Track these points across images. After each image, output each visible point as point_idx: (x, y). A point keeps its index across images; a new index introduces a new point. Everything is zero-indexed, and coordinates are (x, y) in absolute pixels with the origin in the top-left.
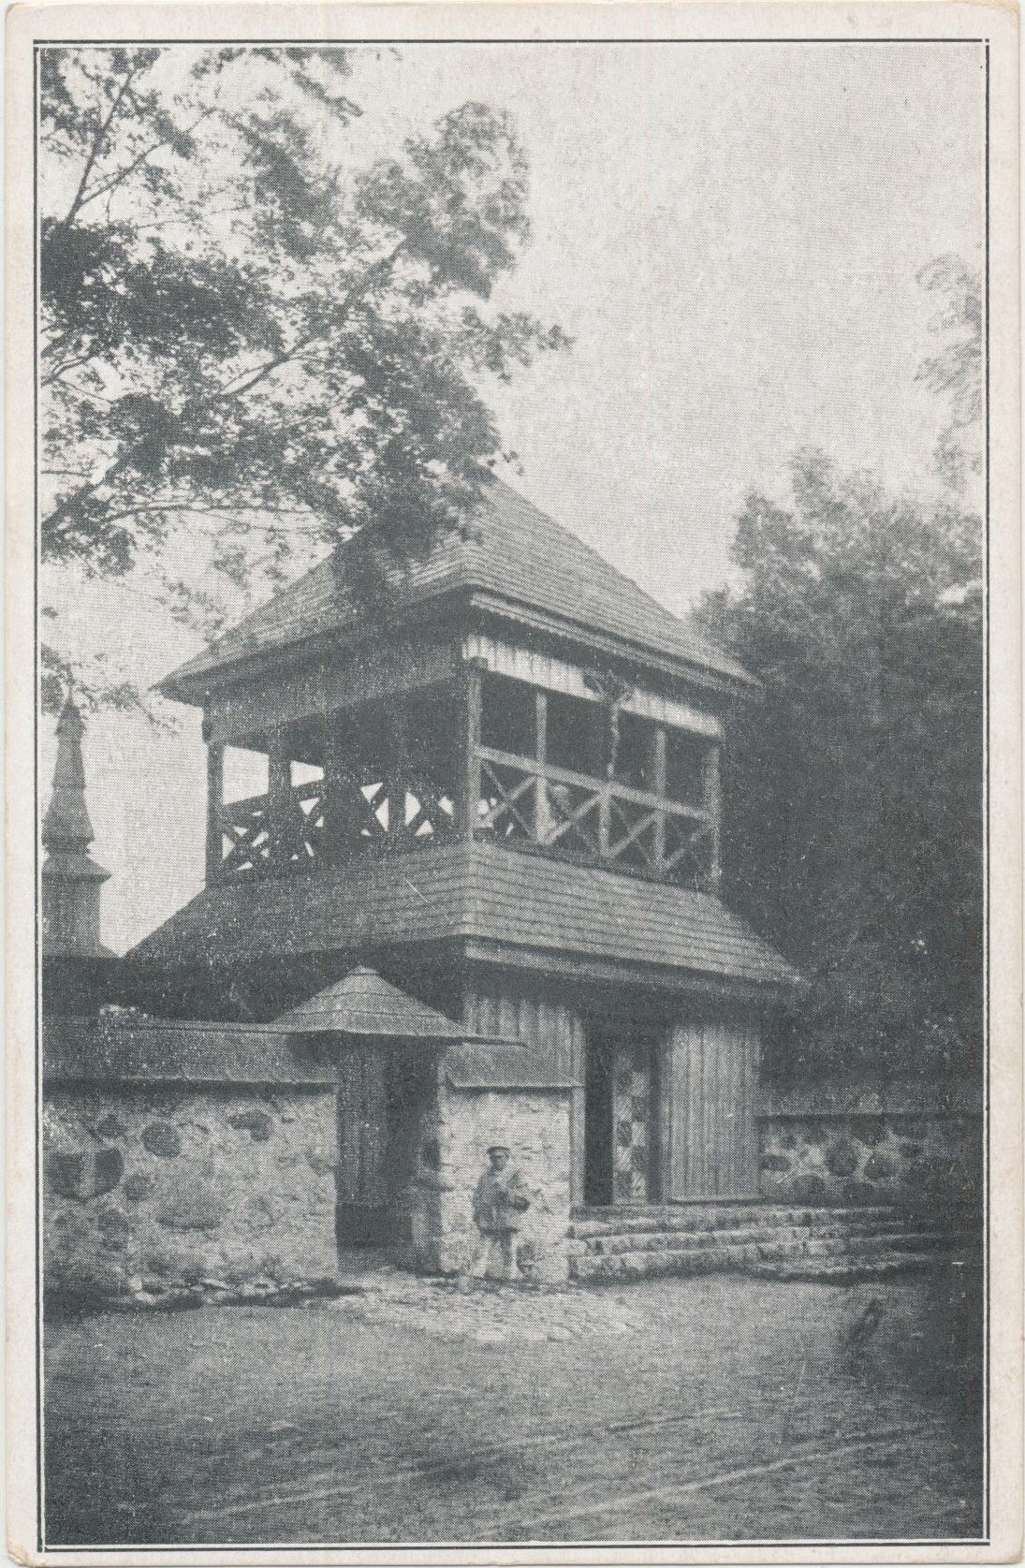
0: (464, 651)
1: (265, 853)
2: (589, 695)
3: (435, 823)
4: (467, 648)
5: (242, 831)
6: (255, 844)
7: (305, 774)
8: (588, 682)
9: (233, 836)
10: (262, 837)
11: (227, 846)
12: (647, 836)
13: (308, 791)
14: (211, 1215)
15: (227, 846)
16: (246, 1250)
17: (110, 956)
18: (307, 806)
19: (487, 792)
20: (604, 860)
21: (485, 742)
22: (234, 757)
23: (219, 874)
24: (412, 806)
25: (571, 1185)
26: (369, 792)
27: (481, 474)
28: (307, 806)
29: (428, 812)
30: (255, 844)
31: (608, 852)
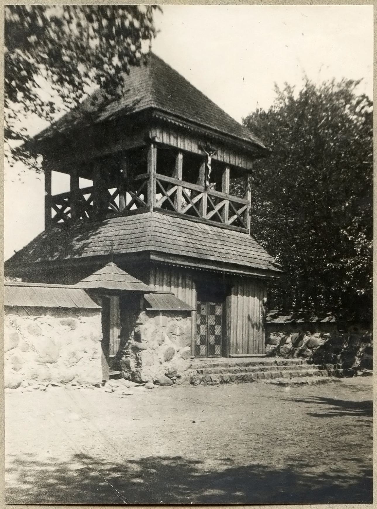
0: (150, 134)
1: (69, 215)
2: (200, 152)
3: (138, 205)
4: (151, 133)
5: (60, 207)
6: (65, 212)
7: (85, 183)
8: (200, 148)
9: (56, 209)
10: (68, 209)
11: (54, 213)
12: (221, 210)
13: (87, 190)
14: (54, 357)
15: (54, 213)
16: (313, 337)
17: (104, 356)
18: (87, 197)
19: (159, 191)
20: (205, 220)
21: (158, 171)
22: (55, 175)
23: (49, 222)
24: (129, 198)
25: (191, 348)
26: (112, 191)
27: (113, 353)
28: (87, 197)
29: (135, 201)
30: (65, 212)
31: (207, 216)
